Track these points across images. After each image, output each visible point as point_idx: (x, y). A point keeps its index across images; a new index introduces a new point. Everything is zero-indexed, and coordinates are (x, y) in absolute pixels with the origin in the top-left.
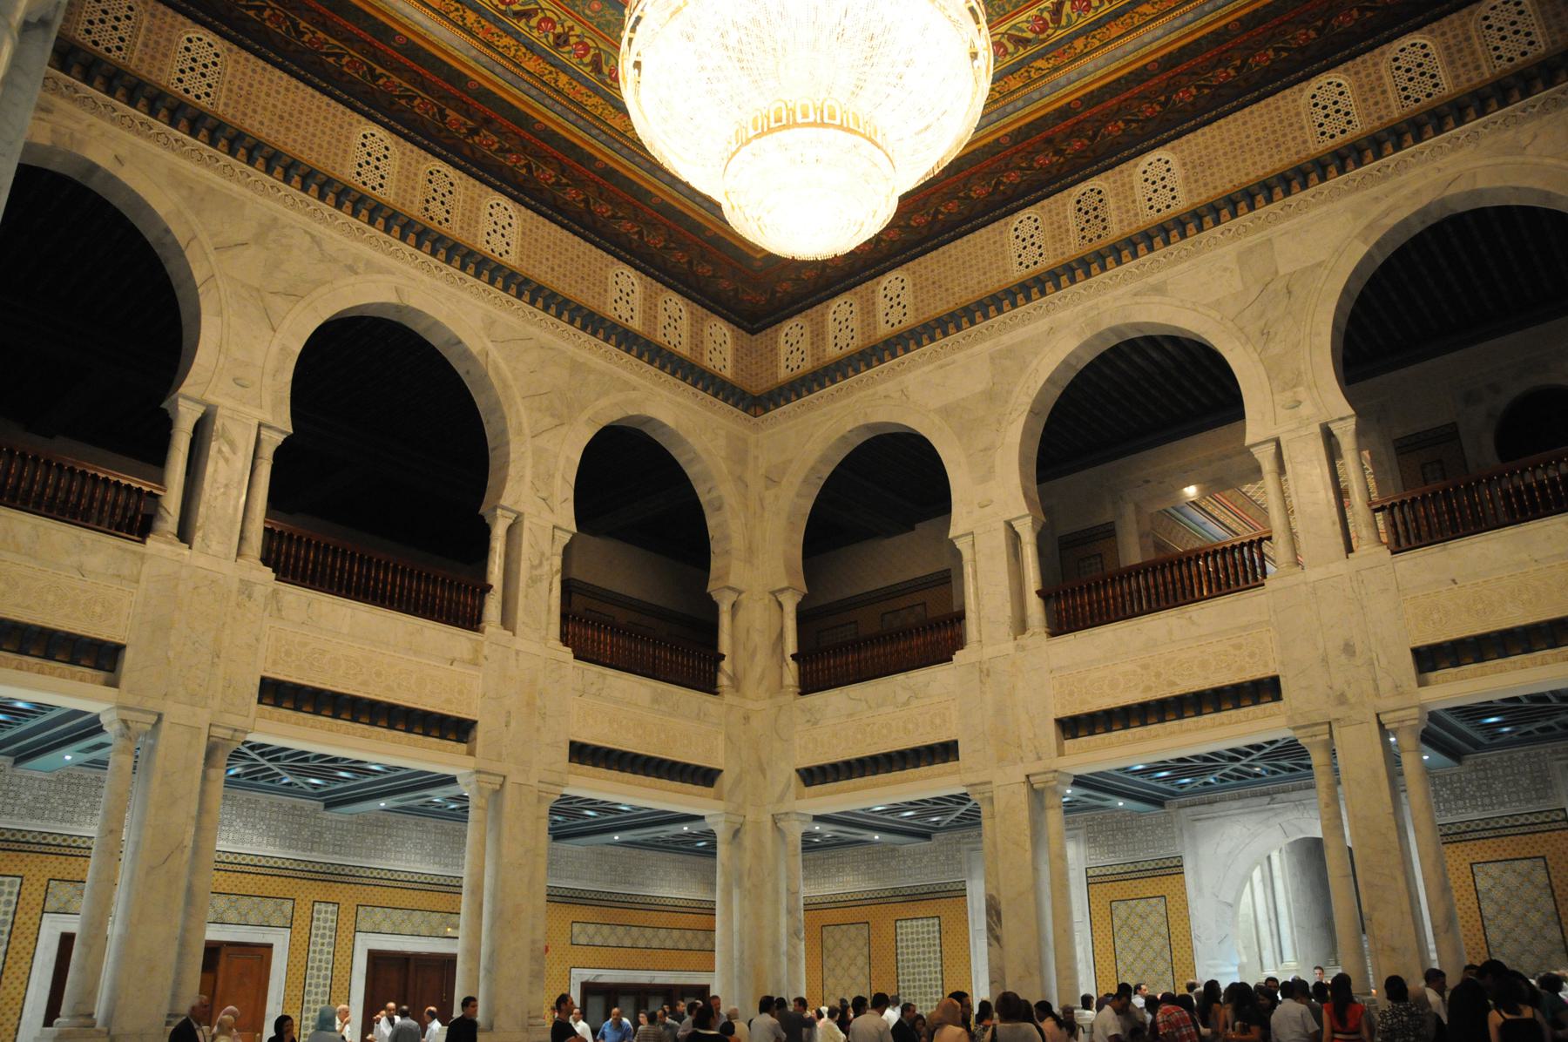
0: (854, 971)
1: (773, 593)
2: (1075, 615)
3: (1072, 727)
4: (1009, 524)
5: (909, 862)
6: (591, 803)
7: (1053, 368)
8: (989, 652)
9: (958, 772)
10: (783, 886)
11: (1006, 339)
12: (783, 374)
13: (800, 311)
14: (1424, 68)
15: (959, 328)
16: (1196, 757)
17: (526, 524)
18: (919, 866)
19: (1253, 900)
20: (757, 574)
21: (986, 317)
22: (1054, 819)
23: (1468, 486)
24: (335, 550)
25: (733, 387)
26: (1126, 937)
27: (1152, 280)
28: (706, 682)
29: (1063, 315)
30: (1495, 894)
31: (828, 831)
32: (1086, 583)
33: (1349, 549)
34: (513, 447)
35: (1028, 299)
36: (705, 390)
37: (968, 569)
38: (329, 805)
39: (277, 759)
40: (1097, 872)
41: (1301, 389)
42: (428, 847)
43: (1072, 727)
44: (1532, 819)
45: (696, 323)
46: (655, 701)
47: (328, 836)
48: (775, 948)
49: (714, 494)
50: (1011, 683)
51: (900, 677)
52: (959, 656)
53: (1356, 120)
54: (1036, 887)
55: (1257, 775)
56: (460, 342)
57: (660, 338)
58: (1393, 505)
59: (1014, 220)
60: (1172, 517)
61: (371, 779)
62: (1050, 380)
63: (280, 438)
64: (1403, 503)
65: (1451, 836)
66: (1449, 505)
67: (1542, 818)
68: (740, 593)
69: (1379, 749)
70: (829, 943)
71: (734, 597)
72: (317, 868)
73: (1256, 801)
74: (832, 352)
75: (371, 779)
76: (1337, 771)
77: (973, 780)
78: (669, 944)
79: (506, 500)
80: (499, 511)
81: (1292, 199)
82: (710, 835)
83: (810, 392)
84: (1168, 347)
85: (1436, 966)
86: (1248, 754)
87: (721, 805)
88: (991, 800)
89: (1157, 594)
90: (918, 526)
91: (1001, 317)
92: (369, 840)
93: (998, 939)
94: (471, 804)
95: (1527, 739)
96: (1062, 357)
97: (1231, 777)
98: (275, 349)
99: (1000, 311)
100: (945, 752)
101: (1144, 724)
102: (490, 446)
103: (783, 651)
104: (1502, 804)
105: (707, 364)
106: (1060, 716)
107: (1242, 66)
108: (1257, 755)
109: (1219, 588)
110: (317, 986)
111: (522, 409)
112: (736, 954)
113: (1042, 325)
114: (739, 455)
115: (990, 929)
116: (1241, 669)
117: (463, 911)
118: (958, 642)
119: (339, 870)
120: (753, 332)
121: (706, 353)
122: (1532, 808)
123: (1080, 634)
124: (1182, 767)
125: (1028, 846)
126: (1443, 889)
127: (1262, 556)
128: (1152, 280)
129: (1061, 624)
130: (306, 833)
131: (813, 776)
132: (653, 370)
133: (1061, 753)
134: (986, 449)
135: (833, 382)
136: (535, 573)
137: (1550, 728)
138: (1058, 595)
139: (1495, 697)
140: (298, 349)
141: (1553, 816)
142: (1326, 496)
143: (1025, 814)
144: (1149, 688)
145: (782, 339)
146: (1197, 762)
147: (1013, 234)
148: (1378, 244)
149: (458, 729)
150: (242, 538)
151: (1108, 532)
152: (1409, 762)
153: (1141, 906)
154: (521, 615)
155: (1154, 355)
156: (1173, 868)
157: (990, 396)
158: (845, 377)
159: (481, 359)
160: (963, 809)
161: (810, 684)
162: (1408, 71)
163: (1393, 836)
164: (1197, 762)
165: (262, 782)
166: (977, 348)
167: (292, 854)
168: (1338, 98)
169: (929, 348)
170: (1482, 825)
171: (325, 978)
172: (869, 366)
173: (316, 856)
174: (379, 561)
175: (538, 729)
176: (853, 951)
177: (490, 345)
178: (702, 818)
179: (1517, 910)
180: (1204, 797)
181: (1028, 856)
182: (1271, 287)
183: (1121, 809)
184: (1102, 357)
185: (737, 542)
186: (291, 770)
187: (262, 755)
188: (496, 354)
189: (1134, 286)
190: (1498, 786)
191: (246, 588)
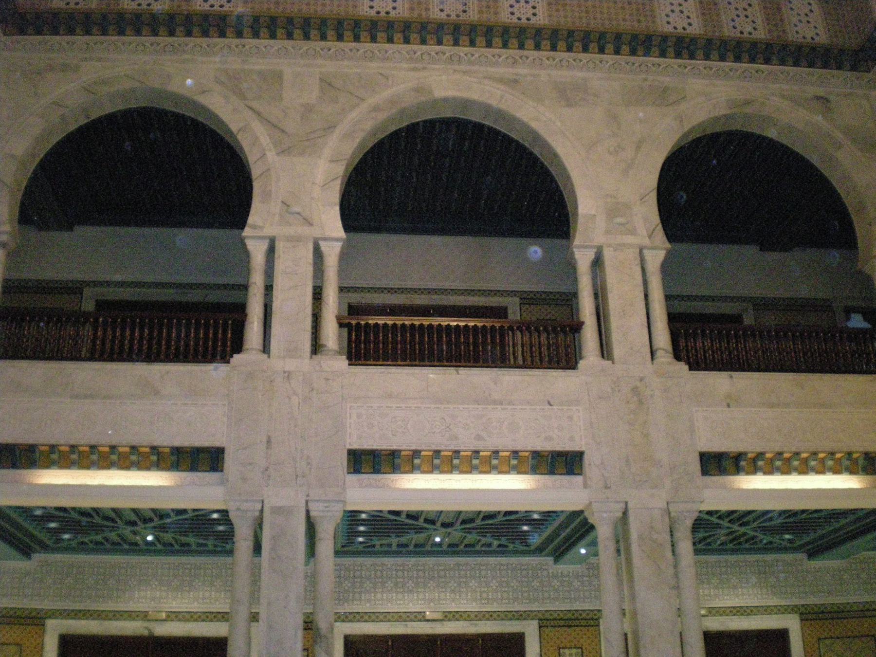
16: (74, 509)
91: (171, 39)
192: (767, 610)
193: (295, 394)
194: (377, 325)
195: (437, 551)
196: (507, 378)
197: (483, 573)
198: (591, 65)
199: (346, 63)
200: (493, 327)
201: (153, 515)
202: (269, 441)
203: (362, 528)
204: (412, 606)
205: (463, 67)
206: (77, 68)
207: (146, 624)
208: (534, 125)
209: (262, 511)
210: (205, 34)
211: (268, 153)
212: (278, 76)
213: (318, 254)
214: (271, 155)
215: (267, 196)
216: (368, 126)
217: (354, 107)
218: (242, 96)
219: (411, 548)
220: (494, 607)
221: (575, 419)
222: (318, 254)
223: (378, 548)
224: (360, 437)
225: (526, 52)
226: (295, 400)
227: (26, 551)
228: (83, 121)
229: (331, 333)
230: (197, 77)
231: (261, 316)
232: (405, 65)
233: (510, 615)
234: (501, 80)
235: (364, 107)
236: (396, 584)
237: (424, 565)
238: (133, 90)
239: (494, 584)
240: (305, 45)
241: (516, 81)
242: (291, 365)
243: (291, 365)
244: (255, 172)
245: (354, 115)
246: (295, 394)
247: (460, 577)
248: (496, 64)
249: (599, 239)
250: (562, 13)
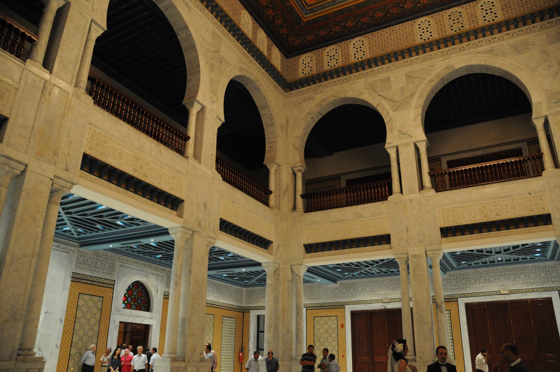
14: (492, 10)
16: (343, 264)
20: (285, 155)
38: (82, 245)
53: (499, 16)
55: (373, 273)
59: (419, 21)
81: (464, 44)
91: (345, 77)
97: (363, 273)
107: (358, 22)
108: (375, 265)
116: (532, 210)
120: (287, 58)
145: (301, 62)
147: (352, 46)
162: (486, 10)
164: (343, 266)
168: (428, 26)
192: (533, 290)
193: (415, 208)
194: (465, 169)
195: (500, 263)
196: (507, 186)
197: (526, 271)
198: (529, 31)
199: (415, 66)
200: (520, 160)
201: (372, 263)
202: (407, 229)
203: (538, 250)
204: (494, 287)
205: (466, 52)
206: (313, 98)
207: (383, 304)
208: (504, 68)
209: (408, 258)
210: (357, 71)
211: (390, 112)
212: (388, 79)
213: (417, 149)
214: (391, 113)
215: (392, 129)
216: (429, 89)
217: (421, 83)
218: (375, 91)
219: (512, 261)
220: (534, 286)
221: (544, 199)
222: (417, 149)
223: (520, 260)
224: (444, 222)
225: (494, 36)
226: (415, 211)
227: (335, 281)
228: (320, 117)
229: (300, 202)
230: (357, 88)
231: (398, 178)
232: (441, 59)
233: (543, 290)
234: (485, 52)
235: (425, 82)
236: (485, 280)
237: (497, 270)
238: (335, 100)
239: (533, 276)
240: (397, 63)
241: (492, 50)
242: (411, 196)
243: (411, 196)
244: (386, 121)
245: (422, 86)
246: (415, 208)
247: (515, 274)
248: (481, 46)
249: (545, 113)
250: (510, 11)
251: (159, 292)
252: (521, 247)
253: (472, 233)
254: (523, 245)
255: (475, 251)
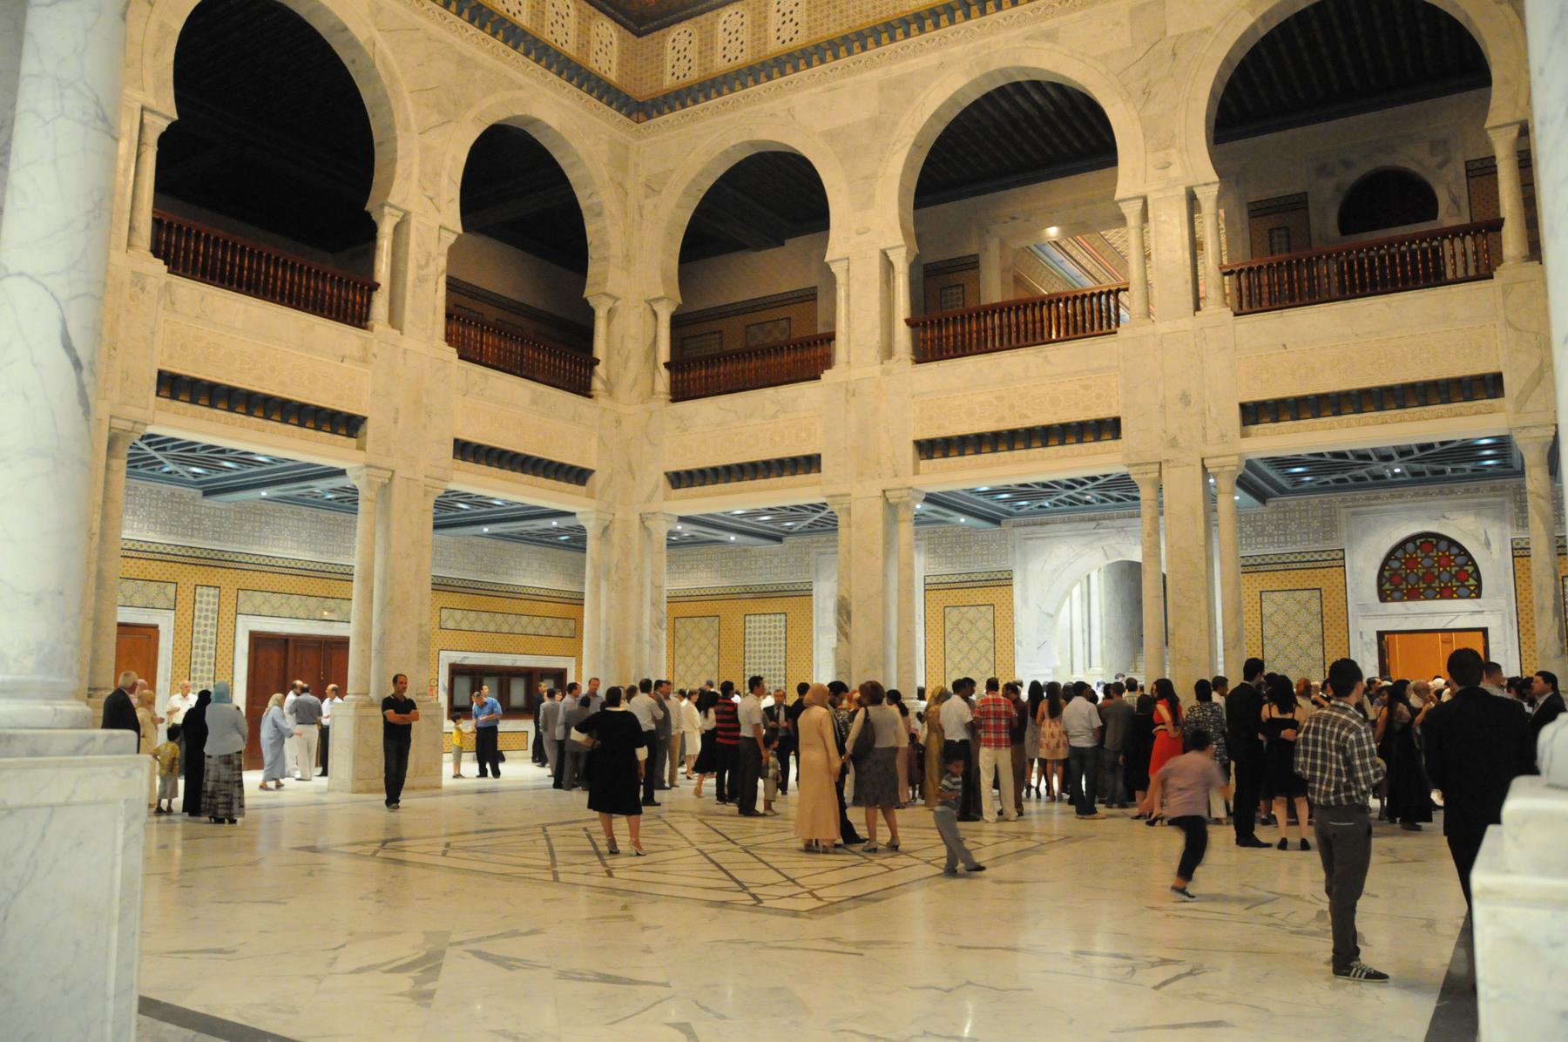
0: (703, 660)
1: (649, 302)
2: (940, 346)
3: (928, 448)
4: (884, 254)
5: (761, 562)
6: (467, 497)
7: (940, 103)
8: (855, 374)
9: (818, 483)
10: (647, 581)
11: (896, 69)
12: (669, 82)
13: (689, 17)
15: (850, 53)
17: (414, 223)
18: (770, 566)
19: (1071, 613)
20: (633, 283)
21: (878, 43)
22: (906, 530)
23: (1309, 260)
24: (225, 243)
25: (618, 92)
26: (956, 639)
27: (1045, 25)
28: (582, 387)
29: (955, 50)
30: (1276, 618)
31: (685, 530)
32: (950, 316)
33: (1197, 308)
34: (400, 144)
35: (922, 30)
36: (590, 92)
37: (841, 294)
38: (207, 493)
39: (164, 449)
40: (935, 580)
41: (1173, 151)
42: (304, 535)
43: (928, 448)
44: (1316, 556)
45: (583, 21)
46: (534, 402)
47: (207, 523)
48: (639, 636)
49: (595, 199)
50: (872, 402)
51: (770, 391)
52: (827, 375)
54: (884, 591)
55: (1087, 502)
56: (345, 29)
57: (547, 37)
58: (1241, 271)
60: (1031, 254)
61: (255, 469)
62: (936, 115)
63: (164, 125)
64: (1250, 269)
65: (1250, 567)
66: (1290, 276)
67: (1324, 556)
68: (617, 299)
69: (1200, 488)
70: (681, 633)
71: (610, 303)
72: (198, 553)
73: (1084, 525)
74: (720, 65)
75: (255, 469)
76: (1161, 504)
77: (832, 492)
78: (530, 630)
79: (393, 199)
80: (386, 209)
82: (581, 529)
83: (696, 102)
84: (1052, 92)
85: (1221, 674)
86: (1083, 484)
87: (593, 503)
88: (849, 511)
89: (1018, 333)
90: (788, 242)
92: (248, 527)
93: (846, 635)
94: (360, 497)
95: (1324, 488)
96: (950, 92)
98: (153, 26)
99: (893, 39)
100: (809, 463)
101: (994, 450)
102: (376, 140)
103: (655, 360)
104: (1294, 543)
105: (592, 65)
106: (919, 438)
108: (1091, 485)
109: (1075, 331)
110: (203, 664)
111: (409, 105)
112: (603, 641)
113: (933, 58)
114: (621, 162)
115: (840, 627)
117: (354, 597)
118: (827, 362)
119: (220, 556)
120: (639, 35)
121: (592, 54)
122: (1318, 547)
123: (942, 363)
124: (1023, 491)
125: (880, 554)
126: (1236, 612)
127: (1117, 301)
128: (1045, 25)
129: (925, 352)
130: (185, 519)
131: (680, 479)
132: (539, 69)
133: (916, 472)
134: (866, 178)
135: (720, 94)
136: (424, 273)
137: (1344, 480)
138: (925, 324)
139: (1304, 452)
140: (178, 26)
141: (1333, 555)
142: (1183, 255)
143: (878, 525)
144: (1002, 419)
145: (669, 45)
146: (1037, 488)
148: (1264, 18)
149: (348, 424)
150: (131, 228)
151: (972, 264)
152: (1224, 504)
153: (972, 613)
154: (408, 315)
155: (1037, 98)
156: (1003, 581)
157: (876, 125)
158: (732, 90)
159: (368, 49)
160: (817, 517)
161: (680, 393)
163: (1202, 565)
164: (1037, 488)
165: (142, 470)
166: (867, 75)
167: (172, 540)
169: (818, 69)
170: (1275, 559)
171: (210, 657)
172: (757, 82)
173: (196, 542)
174: (269, 256)
175: (425, 427)
176: (704, 642)
177: (377, 35)
178: (573, 514)
179: (1292, 633)
180: (1038, 518)
181: (880, 563)
182: (1157, 47)
183: (963, 525)
184: (988, 97)
185: (616, 250)
186: (174, 459)
187: (149, 444)
188: (383, 45)
189: (1028, 29)
190: (1293, 526)
191: (139, 280)
229: (903, 334)
251: (1495, 546)
252: (1438, 448)
253: (1360, 410)
254: (1442, 443)
255: (1416, 451)
